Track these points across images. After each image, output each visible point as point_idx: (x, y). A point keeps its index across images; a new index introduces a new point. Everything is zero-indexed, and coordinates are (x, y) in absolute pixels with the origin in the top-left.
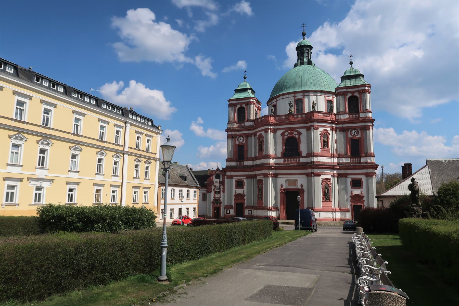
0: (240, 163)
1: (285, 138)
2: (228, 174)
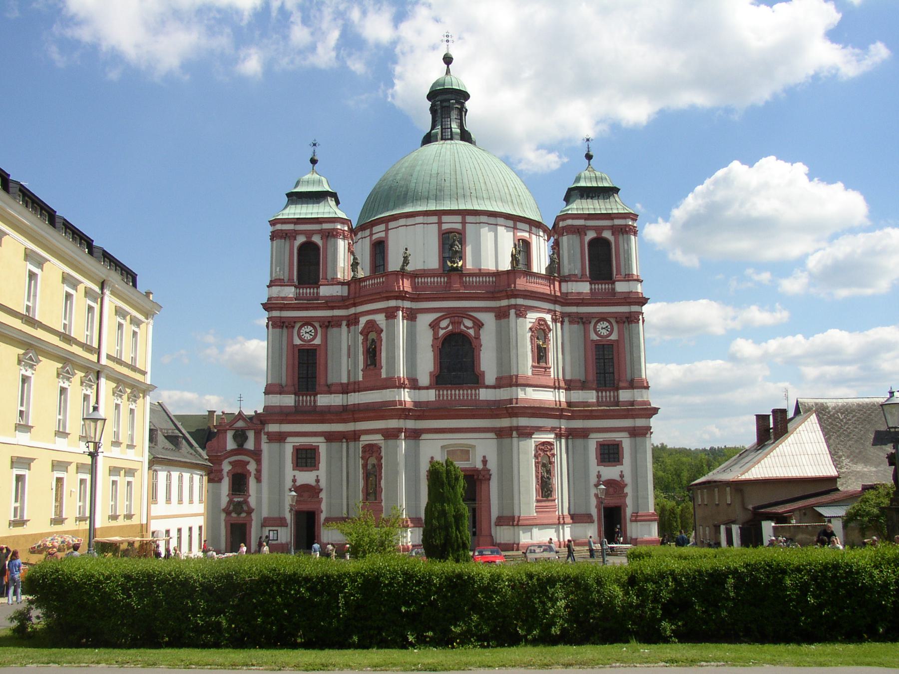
0: (306, 400)
1: (440, 335)
2: (273, 428)
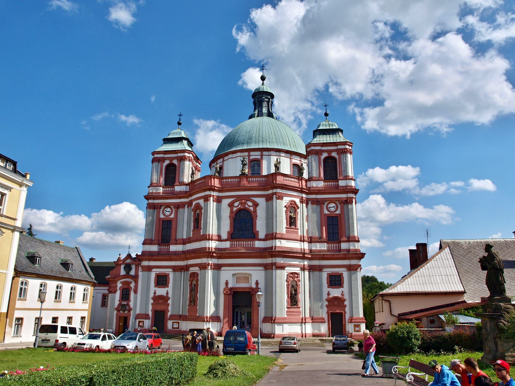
2: (145, 263)
